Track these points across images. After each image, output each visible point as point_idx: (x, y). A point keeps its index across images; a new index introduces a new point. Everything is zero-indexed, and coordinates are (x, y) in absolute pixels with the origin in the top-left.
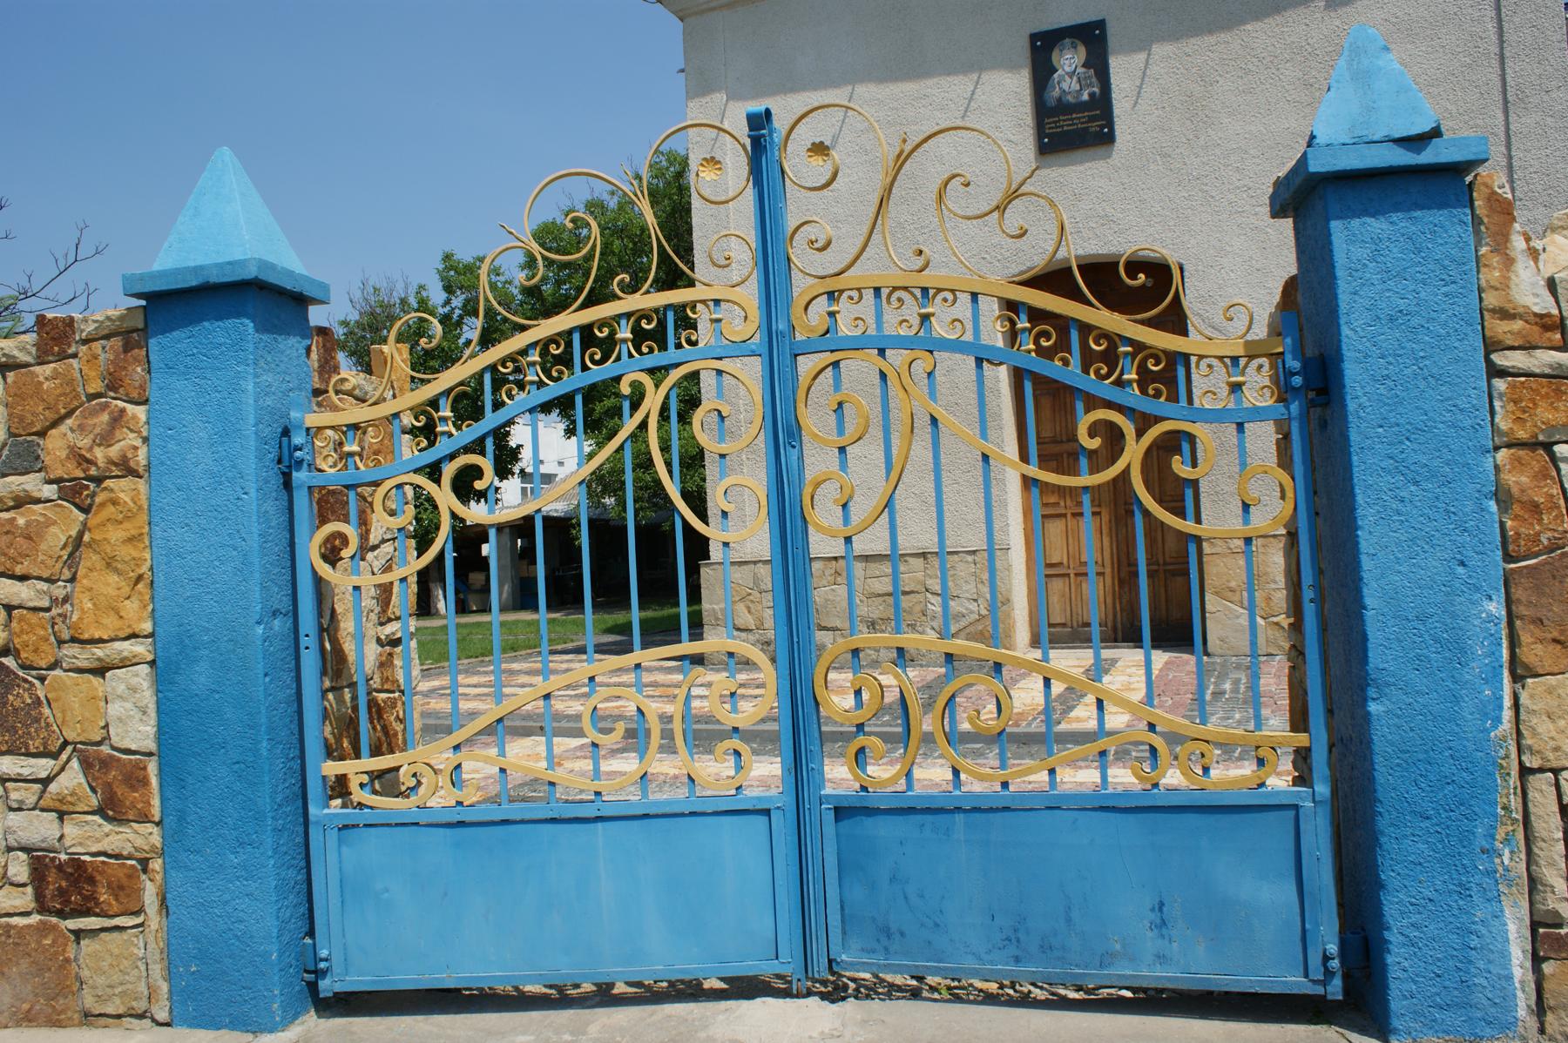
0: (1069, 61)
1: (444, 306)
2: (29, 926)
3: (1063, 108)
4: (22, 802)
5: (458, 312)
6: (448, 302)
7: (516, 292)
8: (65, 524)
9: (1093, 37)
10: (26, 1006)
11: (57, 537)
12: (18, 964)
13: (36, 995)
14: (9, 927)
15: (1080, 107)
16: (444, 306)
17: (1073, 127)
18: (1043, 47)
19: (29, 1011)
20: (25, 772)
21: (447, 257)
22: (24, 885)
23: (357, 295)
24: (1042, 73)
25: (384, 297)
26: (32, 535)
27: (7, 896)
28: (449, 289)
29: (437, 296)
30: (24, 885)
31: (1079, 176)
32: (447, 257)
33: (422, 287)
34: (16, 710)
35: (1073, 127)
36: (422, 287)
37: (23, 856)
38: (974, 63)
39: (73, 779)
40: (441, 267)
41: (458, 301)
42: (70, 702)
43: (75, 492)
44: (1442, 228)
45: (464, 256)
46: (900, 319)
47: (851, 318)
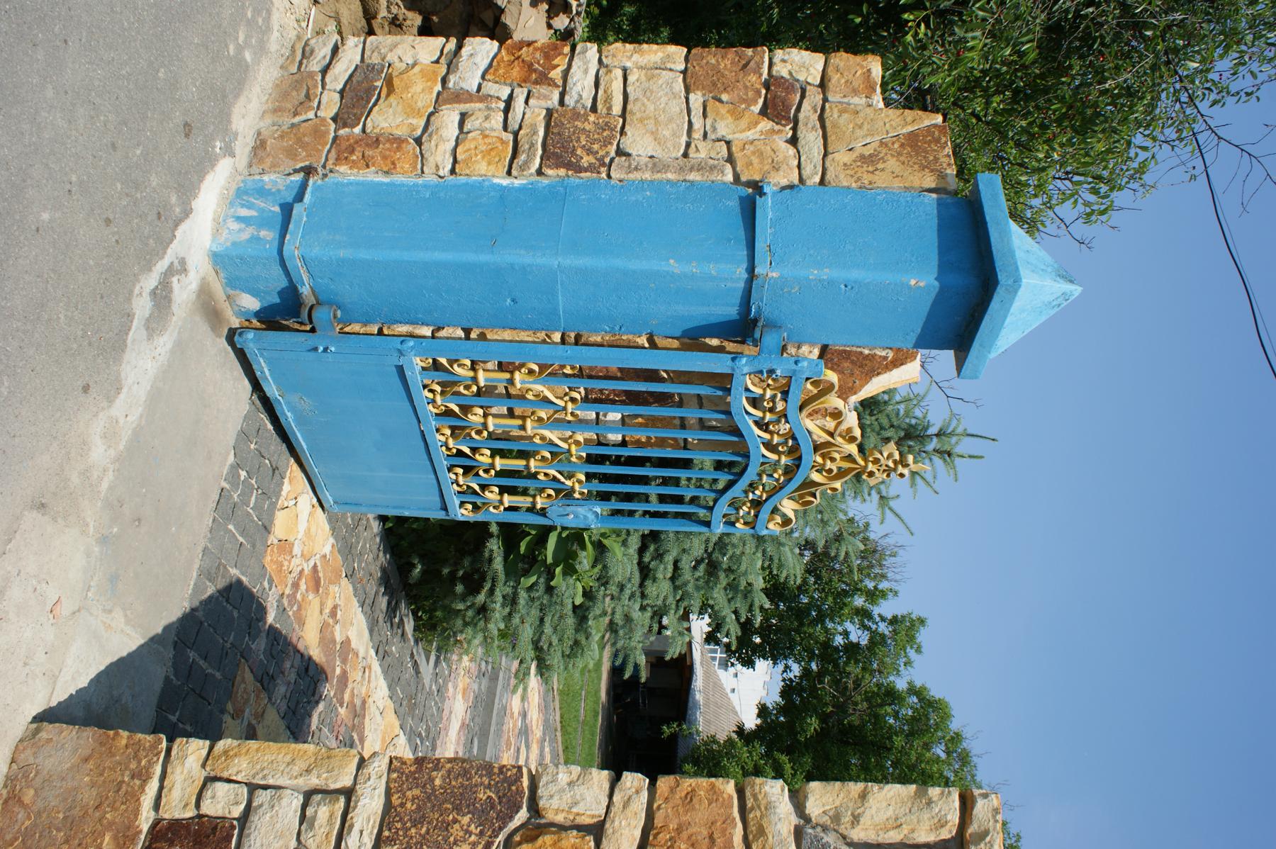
1: (880, 615)
2: (136, 812)
4: (311, 826)
5: (874, 627)
6: (883, 619)
7: (892, 678)
10: (28, 796)
12: (93, 784)
13: (39, 814)
14: (144, 776)
16: (880, 615)
19: (20, 801)
21: (922, 621)
22: (198, 806)
23: (890, 541)
25: (888, 562)
27: (190, 777)
28: (894, 621)
29: (886, 608)
30: (198, 806)
32: (922, 621)
33: (896, 593)
34: (447, 826)
36: (896, 593)
37: (237, 811)
40: (914, 617)
41: (883, 628)
45: (923, 636)
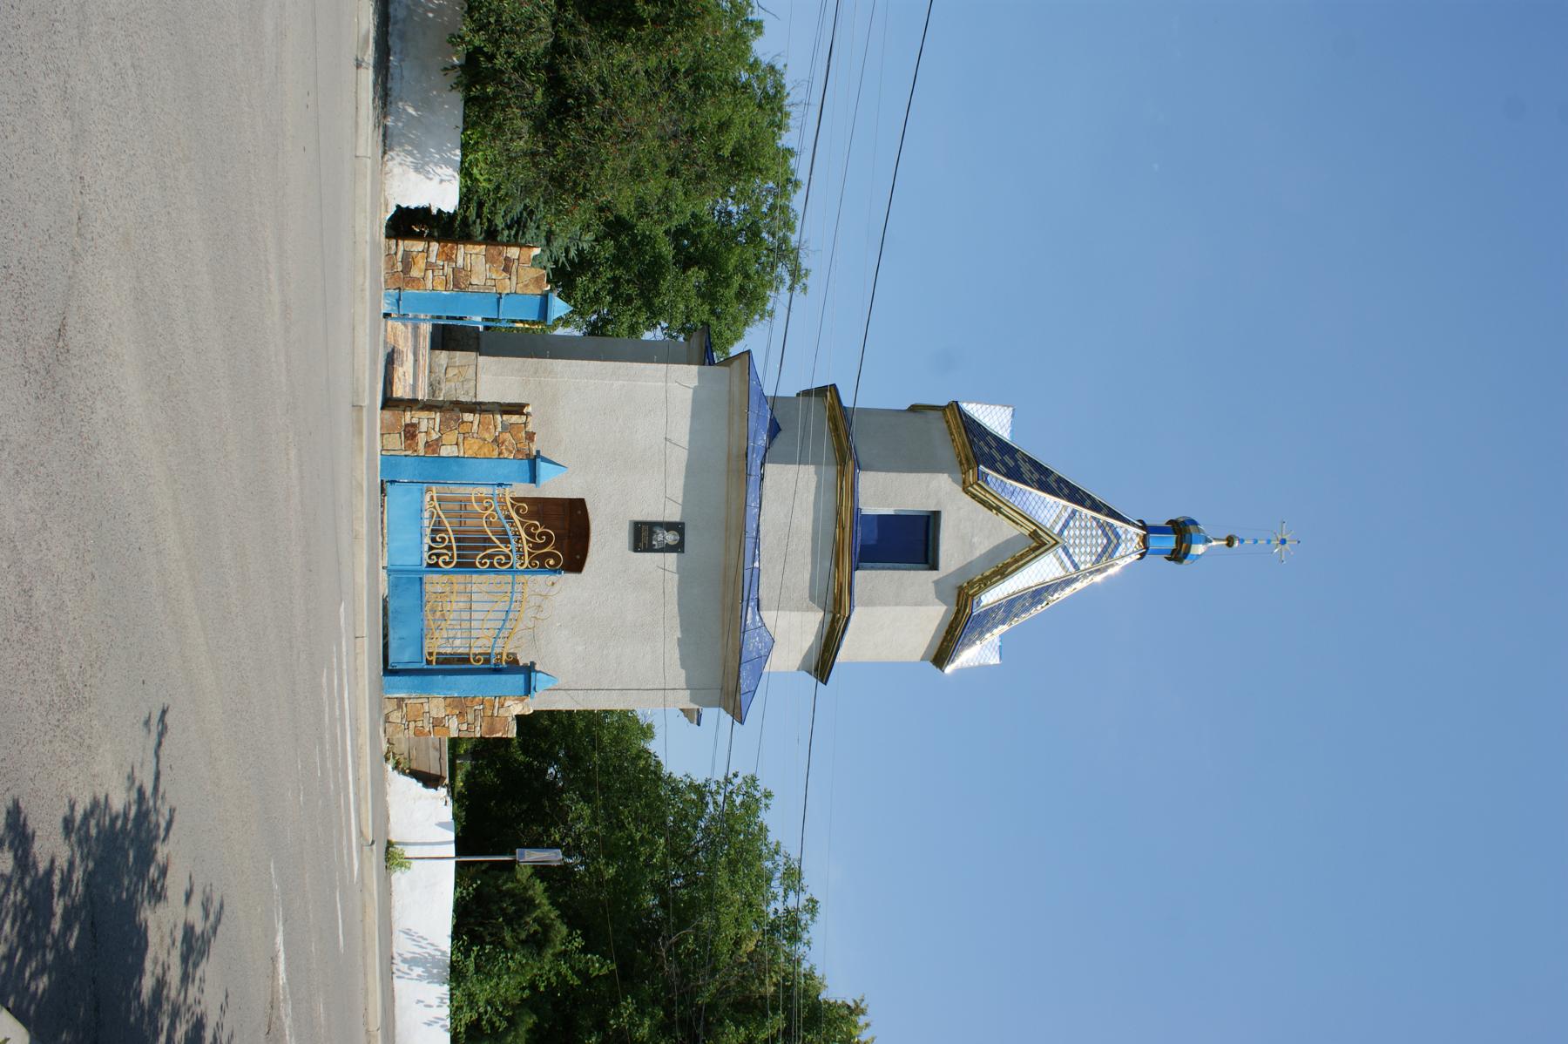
0: (671, 538)
3: (652, 533)
8: (489, 438)
9: (678, 548)
11: (487, 436)
15: (651, 540)
17: (643, 536)
18: (677, 527)
20: (362, 782)
24: (669, 526)
26: (487, 429)
31: (624, 537)
35: (643, 536)
38: (684, 505)
39: (435, 436)
42: (451, 437)
43: (495, 440)
44: (522, 691)
46: (517, 596)
47: (518, 588)
